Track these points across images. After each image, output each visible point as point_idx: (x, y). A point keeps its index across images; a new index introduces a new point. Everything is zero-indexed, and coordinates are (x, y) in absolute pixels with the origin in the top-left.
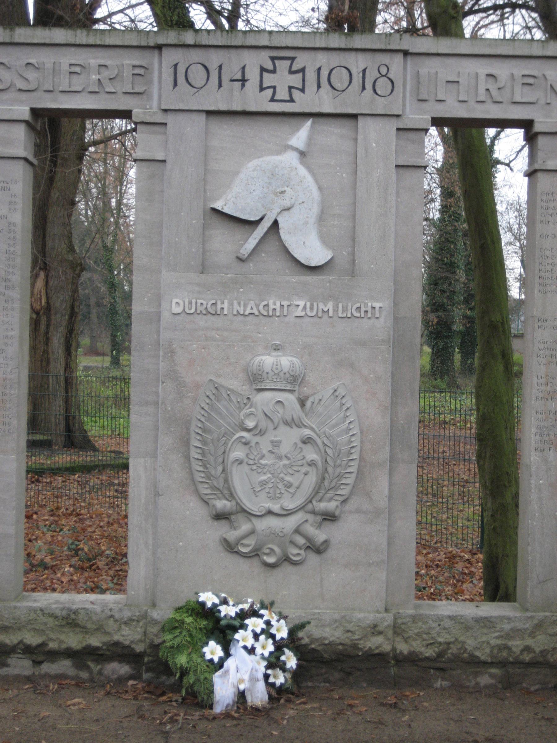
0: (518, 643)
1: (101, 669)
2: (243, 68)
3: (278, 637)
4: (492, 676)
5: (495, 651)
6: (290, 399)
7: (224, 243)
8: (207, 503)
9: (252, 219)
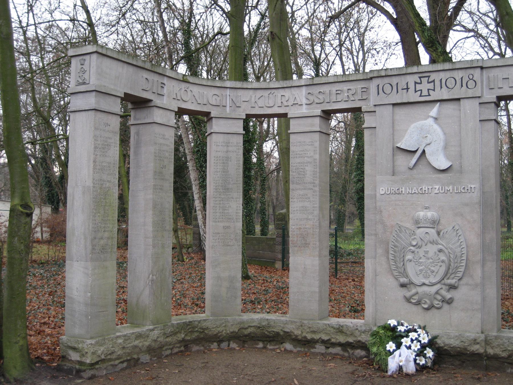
2: (407, 83)
6: (432, 231)
7: (404, 162)
9: (413, 150)
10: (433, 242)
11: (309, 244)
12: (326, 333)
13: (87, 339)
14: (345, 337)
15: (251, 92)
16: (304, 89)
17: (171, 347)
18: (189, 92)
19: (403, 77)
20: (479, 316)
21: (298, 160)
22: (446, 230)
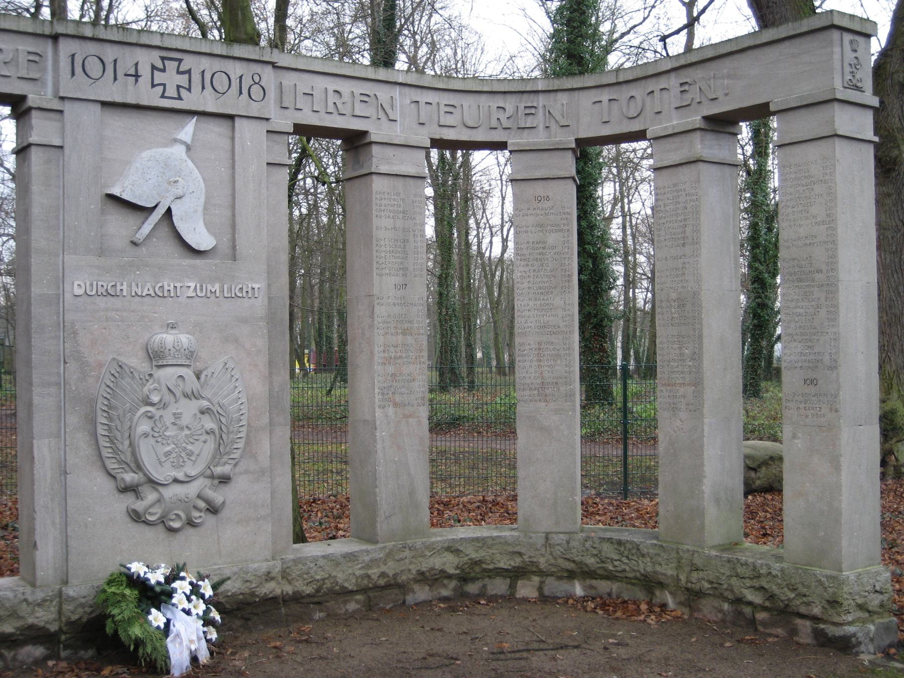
0: (375, 570)
1: (16, 655)
2: (137, 64)
3: (207, 596)
4: (357, 602)
5: (359, 581)
6: (188, 373)
7: (119, 226)
8: (114, 478)
19: (127, 49)
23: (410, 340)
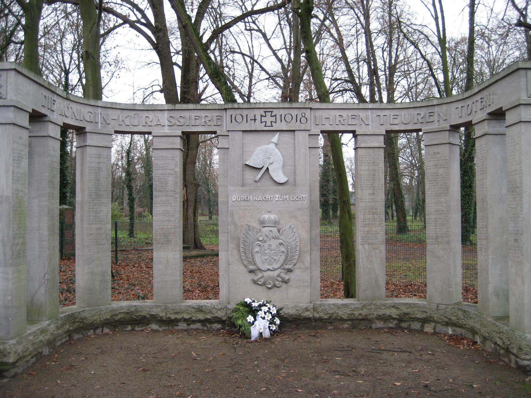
4: (348, 324)
6: (275, 230)
7: (250, 175)
10: (275, 238)
11: (171, 241)
12: (188, 313)
13: (9, 340)
14: (203, 315)
15: (119, 112)
16: (166, 112)
17: (60, 338)
18: (70, 109)
19: (251, 110)
20: (309, 290)
21: (161, 172)
22: (284, 229)
23: (376, 216)
